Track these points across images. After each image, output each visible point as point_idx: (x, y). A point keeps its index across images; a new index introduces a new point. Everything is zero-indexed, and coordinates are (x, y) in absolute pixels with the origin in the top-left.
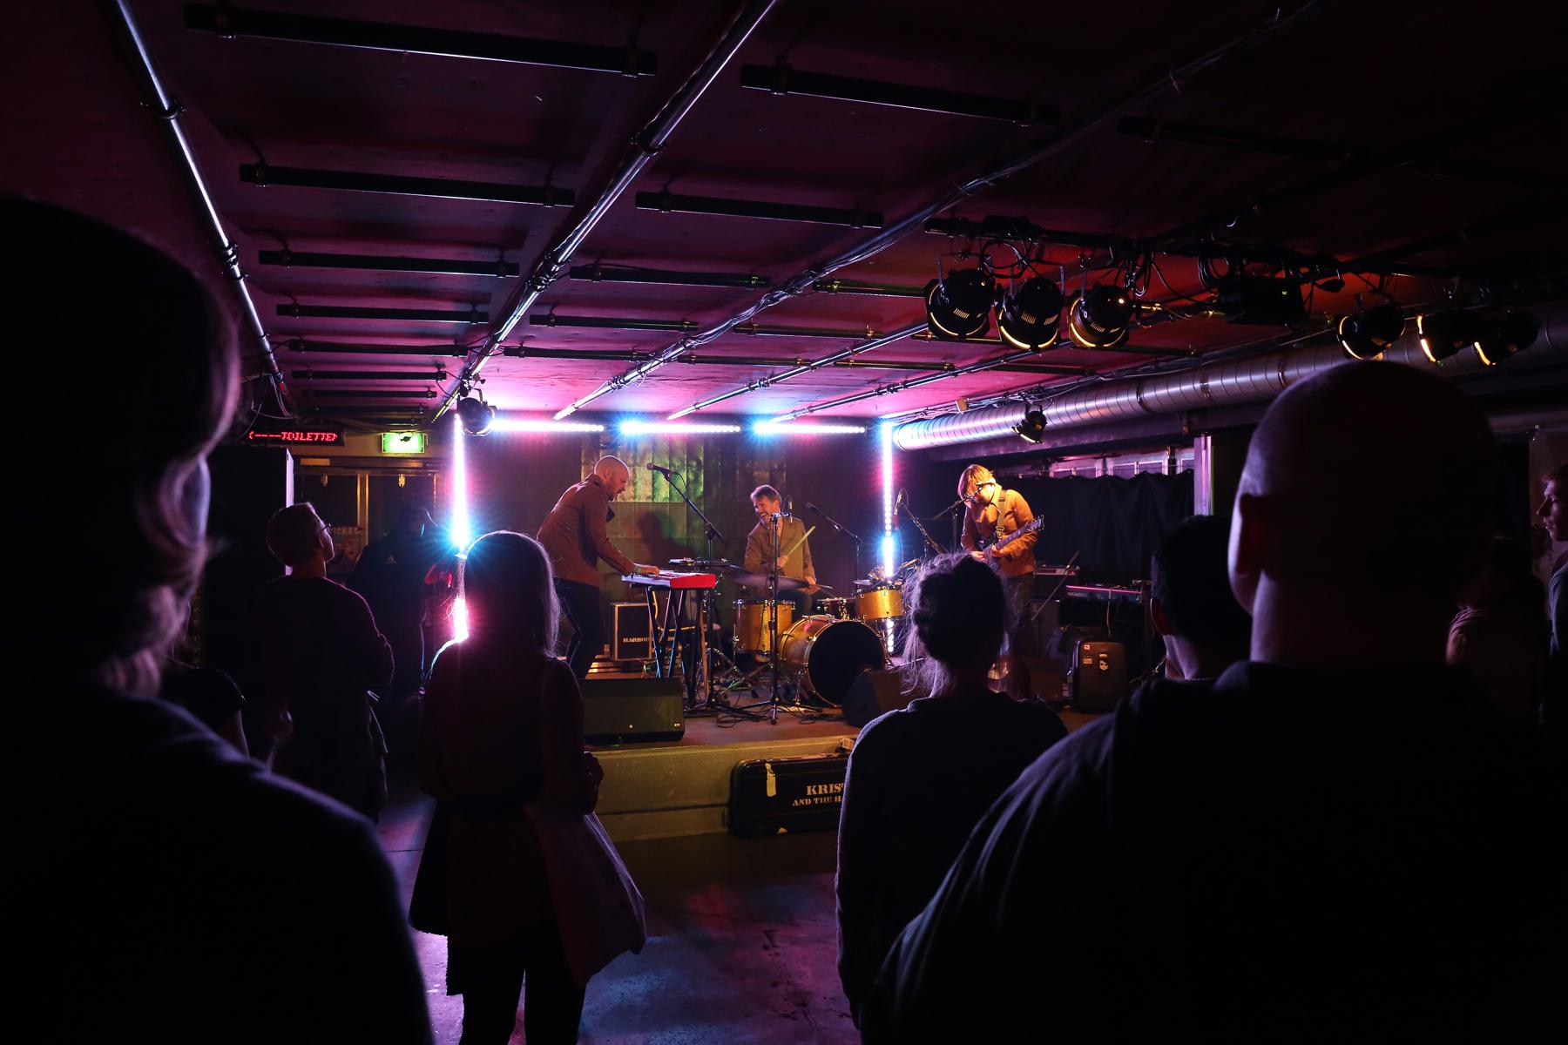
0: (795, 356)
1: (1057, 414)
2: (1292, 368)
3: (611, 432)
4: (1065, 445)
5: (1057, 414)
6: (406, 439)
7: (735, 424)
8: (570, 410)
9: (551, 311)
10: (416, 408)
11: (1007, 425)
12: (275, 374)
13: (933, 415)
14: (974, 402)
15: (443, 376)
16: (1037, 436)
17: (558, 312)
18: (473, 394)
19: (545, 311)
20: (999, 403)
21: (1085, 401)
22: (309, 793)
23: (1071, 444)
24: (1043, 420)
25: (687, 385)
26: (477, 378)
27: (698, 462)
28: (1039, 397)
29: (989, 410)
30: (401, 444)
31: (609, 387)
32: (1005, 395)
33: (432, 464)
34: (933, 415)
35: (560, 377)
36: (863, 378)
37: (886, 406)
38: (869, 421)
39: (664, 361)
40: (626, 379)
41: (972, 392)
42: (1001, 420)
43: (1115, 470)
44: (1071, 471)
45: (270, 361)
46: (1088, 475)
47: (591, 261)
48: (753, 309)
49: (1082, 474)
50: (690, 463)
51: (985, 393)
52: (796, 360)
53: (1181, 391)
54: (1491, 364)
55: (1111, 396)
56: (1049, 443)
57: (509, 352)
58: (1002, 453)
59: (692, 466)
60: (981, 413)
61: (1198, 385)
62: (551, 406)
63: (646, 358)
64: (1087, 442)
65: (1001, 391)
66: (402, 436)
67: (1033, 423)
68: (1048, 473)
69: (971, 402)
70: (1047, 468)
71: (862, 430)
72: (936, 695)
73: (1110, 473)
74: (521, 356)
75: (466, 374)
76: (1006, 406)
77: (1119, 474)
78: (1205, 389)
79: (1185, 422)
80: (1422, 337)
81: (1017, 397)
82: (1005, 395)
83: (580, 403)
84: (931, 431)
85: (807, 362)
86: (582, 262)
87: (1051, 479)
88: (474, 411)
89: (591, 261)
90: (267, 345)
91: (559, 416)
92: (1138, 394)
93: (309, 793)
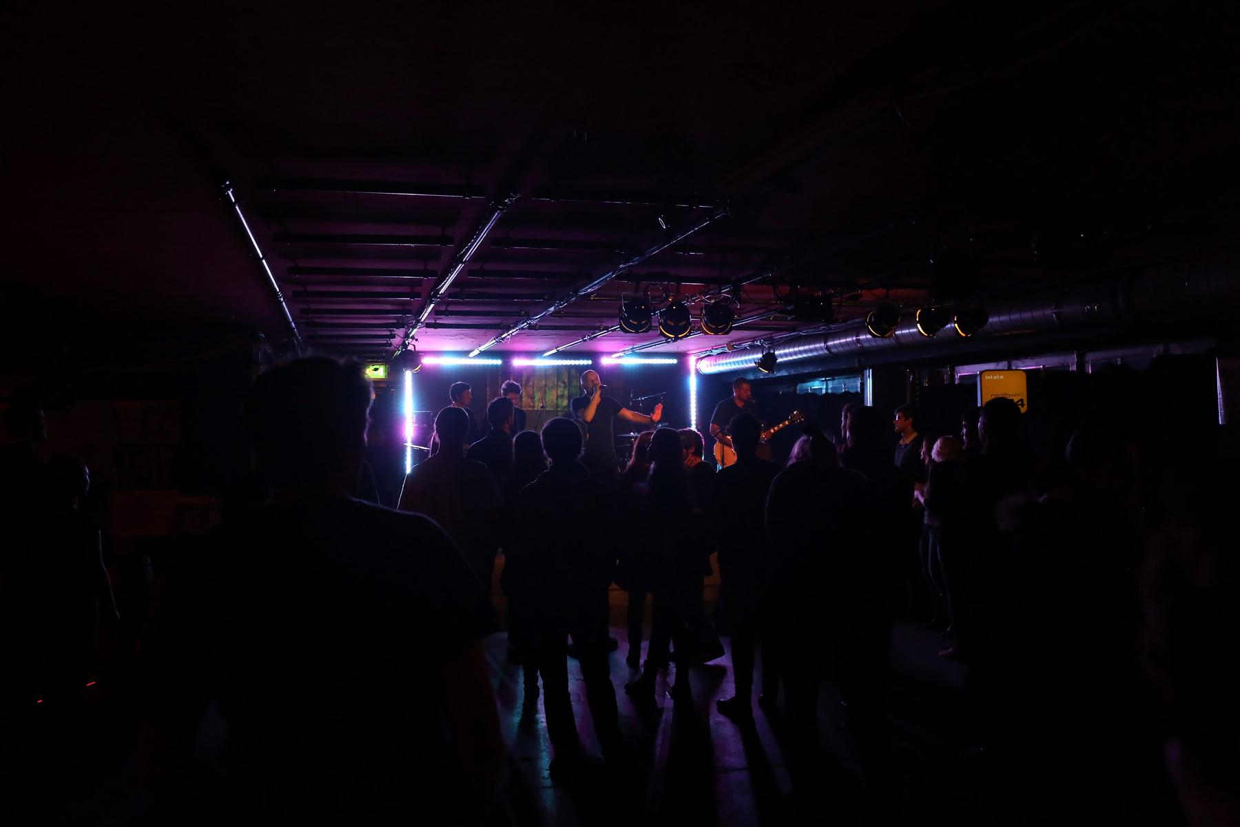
0: (599, 325)
1: (784, 354)
2: (898, 330)
3: (507, 364)
4: (796, 373)
5: (784, 354)
6: (376, 370)
7: (587, 359)
8: (476, 352)
9: (446, 308)
10: (381, 352)
11: (750, 361)
12: (297, 339)
13: (715, 352)
14: (737, 345)
15: (393, 336)
16: (770, 369)
17: (450, 308)
18: (410, 348)
19: (443, 308)
20: (750, 346)
21: (799, 346)
22: (241, 216)
23: (799, 372)
24: (774, 358)
25: (546, 338)
26: (413, 338)
27: (564, 383)
28: (770, 344)
29: (744, 351)
30: (375, 372)
31: (495, 341)
32: (753, 341)
33: (389, 389)
34: (715, 352)
35: (466, 335)
36: (461, 332)
37: (692, 345)
38: (682, 356)
39: (519, 329)
40: (503, 337)
41: (732, 339)
42: (751, 357)
43: (832, 388)
44: (821, 389)
45: (295, 332)
46: (818, 392)
47: (459, 290)
48: (553, 308)
49: (815, 391)
50: (559, 383)
51: (741, 340)
52: (600, 327)
53: (867, 338)
54: (928, 336)
55: (811, 344)
56: (787, 372)
57: (428, 326)
58: (762, 377)
59: (560, 386)
60: (741, 353)
61: (854, 338)
62: (466, 348)
63: (508, 328)
64: (807, 371)
65: (750, 339)
66: (373, 368)
67: (769, 361)
68: (796, 391)
69: (735, 345)
70: (796, 387)
71: (674, 361)
72: (414, 470)
73: (830, 391)
74: (435, 328)
75: (407, 336)
76: (753, 349)
77: (835, 391)
78: (858, 341)
79: (856, 360)
80: (918, 322)
81: (758, 343)
82: (753, 341)
83: (483, 348)
84: (717, 362)
85: (606, 328)
86: (454, 290)
87: (798, 394)
88: (411, 358)
89: (459, 290)
90: (293, 325)
91: (471, 355)
92: (825, 343)
93: (241, 216)
